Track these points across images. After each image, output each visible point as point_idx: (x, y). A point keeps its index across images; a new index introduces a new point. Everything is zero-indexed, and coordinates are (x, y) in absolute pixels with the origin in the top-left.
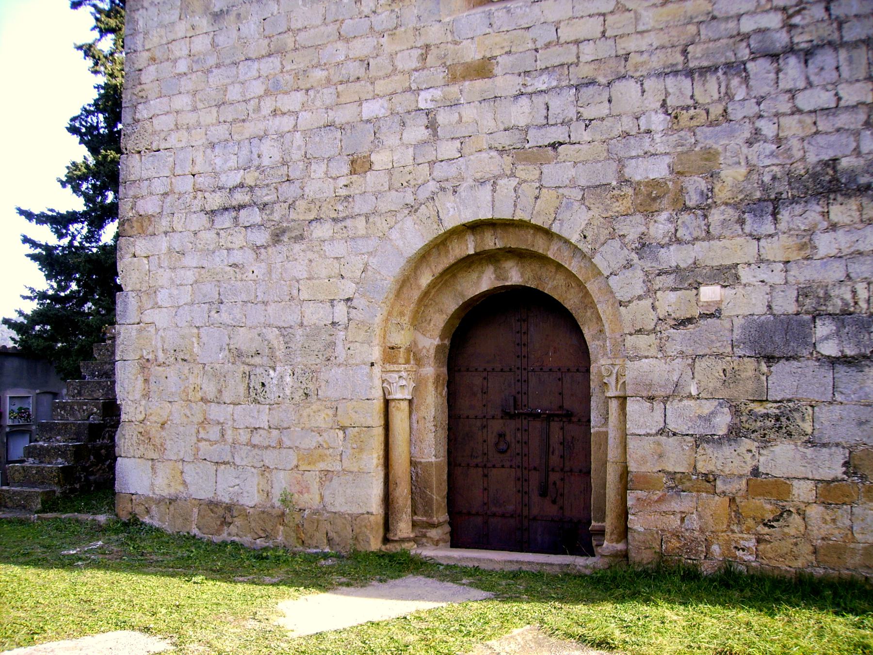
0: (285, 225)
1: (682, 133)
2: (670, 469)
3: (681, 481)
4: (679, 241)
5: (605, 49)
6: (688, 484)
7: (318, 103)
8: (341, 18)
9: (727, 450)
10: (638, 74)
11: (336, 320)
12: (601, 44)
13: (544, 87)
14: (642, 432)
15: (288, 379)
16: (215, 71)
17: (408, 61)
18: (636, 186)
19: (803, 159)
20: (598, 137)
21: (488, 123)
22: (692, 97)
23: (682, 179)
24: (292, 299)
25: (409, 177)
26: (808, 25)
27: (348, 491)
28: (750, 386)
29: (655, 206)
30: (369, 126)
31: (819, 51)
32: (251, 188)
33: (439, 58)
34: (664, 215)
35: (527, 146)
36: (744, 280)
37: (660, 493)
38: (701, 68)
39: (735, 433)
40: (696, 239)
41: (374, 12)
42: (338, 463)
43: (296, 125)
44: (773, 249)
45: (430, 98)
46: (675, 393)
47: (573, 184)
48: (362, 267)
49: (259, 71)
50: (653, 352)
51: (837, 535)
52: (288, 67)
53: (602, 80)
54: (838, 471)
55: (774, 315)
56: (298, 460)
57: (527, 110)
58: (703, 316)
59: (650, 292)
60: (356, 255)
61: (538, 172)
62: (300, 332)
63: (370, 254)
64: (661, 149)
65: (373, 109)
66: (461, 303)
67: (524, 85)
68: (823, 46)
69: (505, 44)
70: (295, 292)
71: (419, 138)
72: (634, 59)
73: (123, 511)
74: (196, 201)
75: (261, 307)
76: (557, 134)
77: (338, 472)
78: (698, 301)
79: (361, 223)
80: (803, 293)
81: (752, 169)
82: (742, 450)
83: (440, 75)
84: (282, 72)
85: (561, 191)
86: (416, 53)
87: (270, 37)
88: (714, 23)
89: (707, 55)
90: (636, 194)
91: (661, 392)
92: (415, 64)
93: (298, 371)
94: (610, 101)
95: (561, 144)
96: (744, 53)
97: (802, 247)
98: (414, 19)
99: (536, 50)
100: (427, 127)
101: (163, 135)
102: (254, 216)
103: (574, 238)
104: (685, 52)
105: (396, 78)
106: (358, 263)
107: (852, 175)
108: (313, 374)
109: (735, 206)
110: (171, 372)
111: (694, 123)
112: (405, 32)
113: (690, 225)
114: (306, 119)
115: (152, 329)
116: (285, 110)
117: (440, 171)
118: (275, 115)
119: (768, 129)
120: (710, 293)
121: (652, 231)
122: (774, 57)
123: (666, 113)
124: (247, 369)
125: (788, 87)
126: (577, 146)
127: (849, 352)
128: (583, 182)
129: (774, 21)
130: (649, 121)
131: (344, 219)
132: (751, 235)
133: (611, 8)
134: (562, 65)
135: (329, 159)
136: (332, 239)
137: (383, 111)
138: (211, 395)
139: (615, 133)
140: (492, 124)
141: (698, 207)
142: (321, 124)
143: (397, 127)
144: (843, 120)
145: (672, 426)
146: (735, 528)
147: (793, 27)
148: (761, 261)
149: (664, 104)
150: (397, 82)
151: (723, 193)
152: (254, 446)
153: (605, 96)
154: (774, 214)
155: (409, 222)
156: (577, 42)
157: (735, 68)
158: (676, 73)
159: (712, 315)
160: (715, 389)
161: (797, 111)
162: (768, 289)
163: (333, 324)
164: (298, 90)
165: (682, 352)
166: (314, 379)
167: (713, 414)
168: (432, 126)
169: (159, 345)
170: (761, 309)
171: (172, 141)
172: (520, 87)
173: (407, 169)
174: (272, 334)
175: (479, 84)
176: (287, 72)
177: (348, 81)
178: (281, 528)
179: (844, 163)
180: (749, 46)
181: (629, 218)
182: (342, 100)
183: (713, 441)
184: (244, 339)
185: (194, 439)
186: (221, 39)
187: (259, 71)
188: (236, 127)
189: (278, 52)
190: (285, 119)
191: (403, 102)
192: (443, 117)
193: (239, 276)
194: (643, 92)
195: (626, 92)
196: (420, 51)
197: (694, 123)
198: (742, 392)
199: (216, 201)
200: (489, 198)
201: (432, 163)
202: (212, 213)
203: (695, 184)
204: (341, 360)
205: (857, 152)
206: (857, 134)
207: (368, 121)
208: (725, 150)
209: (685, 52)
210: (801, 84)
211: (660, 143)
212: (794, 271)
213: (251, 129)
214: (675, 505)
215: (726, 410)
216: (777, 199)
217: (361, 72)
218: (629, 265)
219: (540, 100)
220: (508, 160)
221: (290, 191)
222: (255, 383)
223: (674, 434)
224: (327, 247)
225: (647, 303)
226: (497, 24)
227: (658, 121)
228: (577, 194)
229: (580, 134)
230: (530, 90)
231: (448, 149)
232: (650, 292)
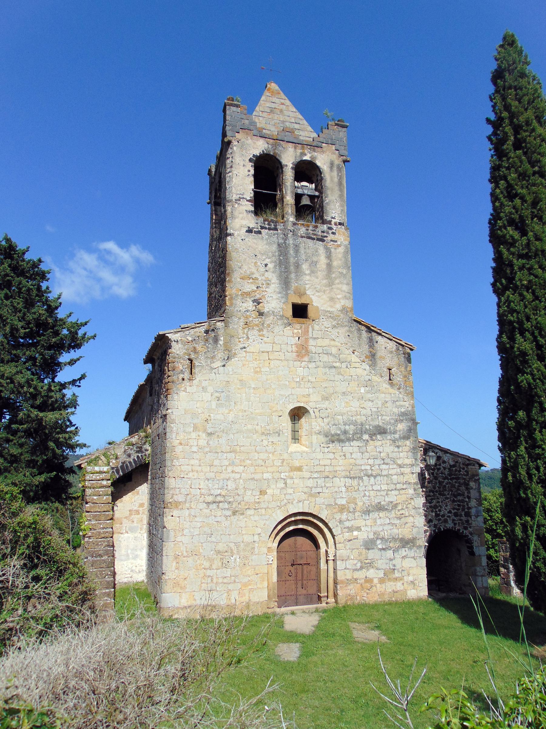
5: (331, 469)
7: (248, 471)
9: (360, 572)
15: (238, 560)
16: (209, 454)
28: (364, 556)
32: (224, 496)
33: (287, 463)
34: (345, 513)
39: (361, 568)
44: (369, 523)
47: (323, 504)
49: (226, 457)
50: (343, 548)
51: (383, 590)
52: (237, 457)
54: (383, 575)
58: (354, 539)
62: (242, 544)
63: (266, 520)
64: (344, 496)
65: (266, 476)
72: (338, 472)
73: (166, 614)
74: (201, 499)
75: (228, 536)
76: (319, 490)
79: (263, 511)
80: (375, 533)
83: (288, 469)
86: (280, 461)
89: (355, 474)
92: (280, 464)
97: (374, 522)
101: (186, 473)
102: (226, 506)
104: (349, 472)
107: (384, 506)
108: (246, 558)
110: (190, 560)
113: (351, 516)
115: (181, 544)
117: (288, 497)
119: (367, 494)
120: (355, 533)
122: (369, 476)
124: (222, 557)
127: (384, 547)
128: (326, 503)
131: (258, 509)
135: (253, 490)
136: (254, 515)
138: (207, 566)
140: (302, 485)
144: (382, 493)
151: (358, 509)
152: (225, 583)
155: (279, 511)
156: (325, 466)
157: (361, 478)
158: (348, 477)
161: (373, 490)
164: (241, 466)
168: (285, 483)
169: (185, 550)
171: (190, 475)
174: (232, 545)
175: (299, 473)
179: (382, 503)
184: (221, 547)
185: (200, 583)
186: (211, 443)
187: (226, 457)
188: (217, 474)
190: (237, 474)
191: (277, 475)
192: (288, 481)
193: (219, 525)
195: (336, 480)
198: (362, 558)
199: (210, 499)
202: (208, 503)
203: (352, 506)
204: (256, 553)
205: (384, 500)
206: (384, 496)
207: (265, 479)
209: (349, 472)
210: (374, 484)
212: (373, 528)
213: (223, 476)
217: (263, 464)
219: (315, 480)
221: (239, 499)
222: (225, 561)
224: (252, 517)
227: (344, 489)
228: (324, 507)
229: (325, 490)
231: (290, 491)
232: (342, 533)
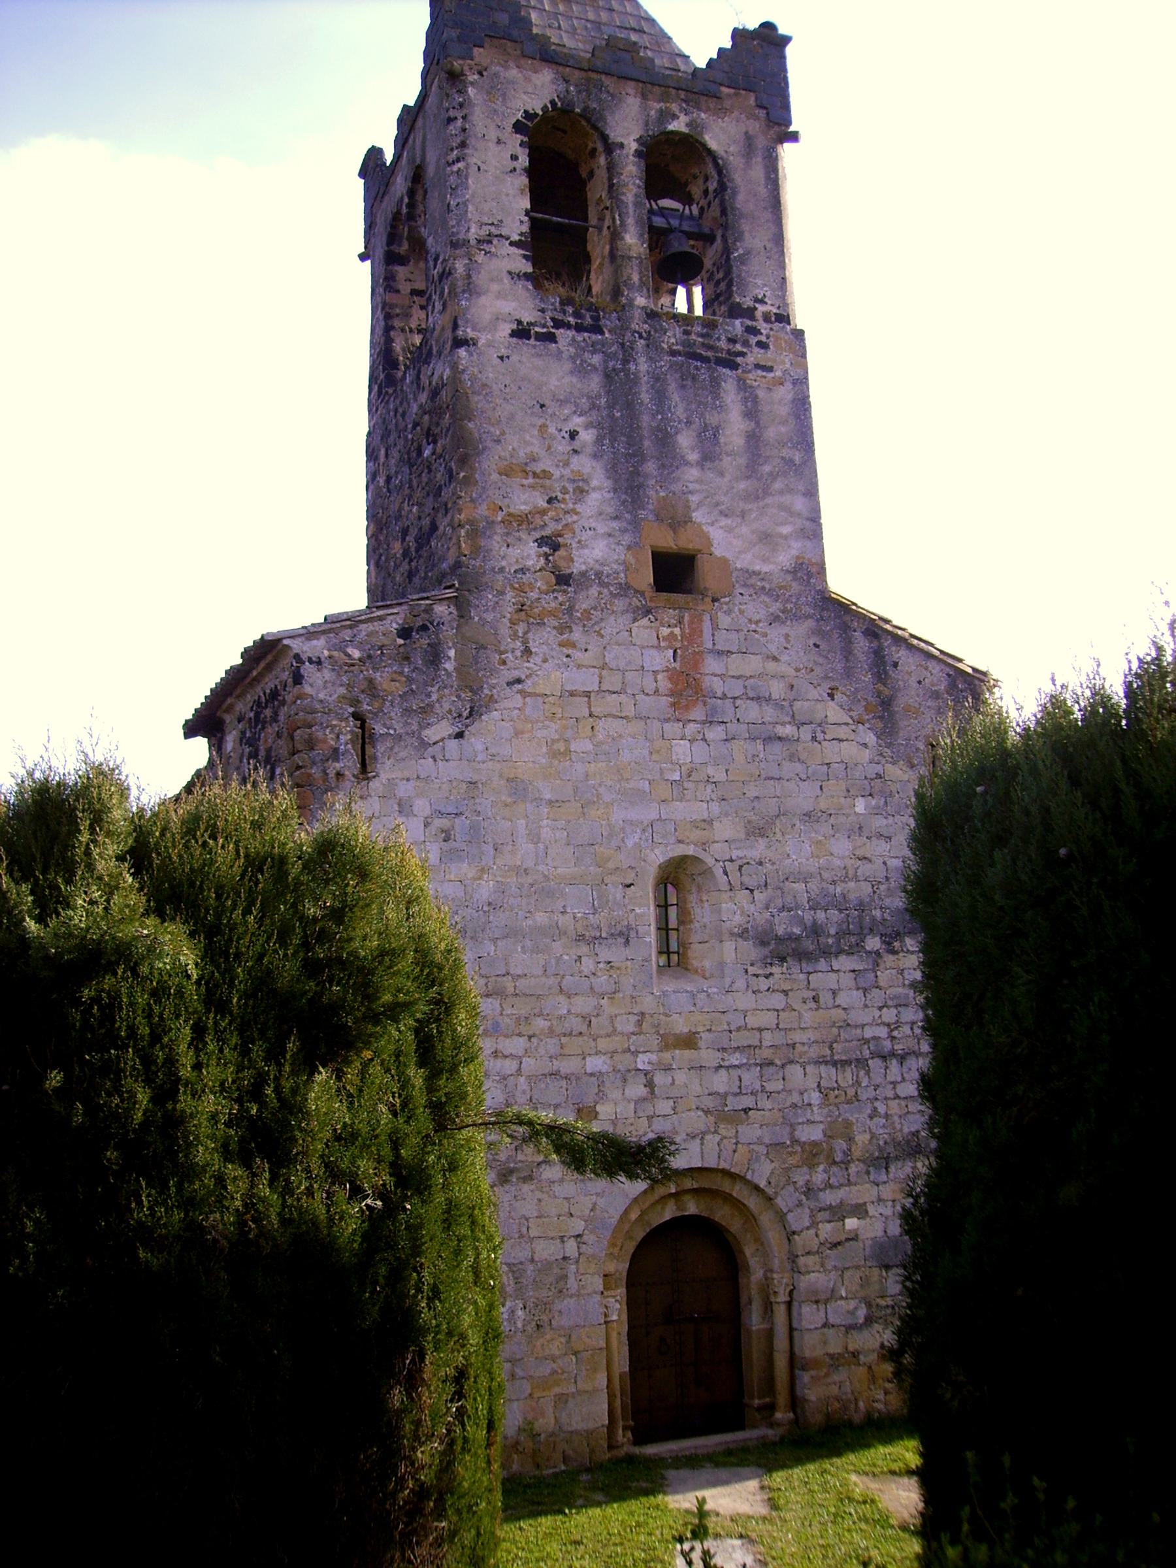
0: (512, 1165)
1: (831, 1108)
2: (831, 1351)
3: (838, 1359)
4: (831, 1187)
5: (779, 1038)
6: (843, 1361)
7: (542, 1051)
8: (561, 973)
9: (866, 1333)
10: (802, 1060)
11: (567, 1255)
12: (776, 1033)
13: (737, 1063)
14: (812, 1327)
17: (627, 1025)
18: (802, 1145)
19: (901, 1130)
20: (776, 1107)
21: (696, 1088)
22: (836, 1081)
23: (831, 1141)
24: (521, 1236)
25: (631, 1128)
26: (902, 1038)
27: (584, 1410)
28: (877, 1287)
29: (816, 1161)
30: (593, 1079)
31: (908, 1057)
34: (821, 1167)
35: (726, 1109)
36: (870, 1214)
37: (825, 1370)
38: (841, 1061)
40: (841, 1185)
41: (594, 974)
42: (573, 1385)
43: (520, 1069)
45: (647, 1061)
46: (833, 1295)
47: (760, 1142)
48: (590, 1206)
50: (817, 1268)
53: (778, 1062)
55: (888, 1237)
56: (532, 1389)
57: (725, 1079)
58: (848, 1240)
59: (814, 1224)
60: (586, 1195)
61: (734, 1131)
62: (531, 1267)
64: (818, 1118)
65: (595, 1063)
66: (648, 1231)
67: (723, 1059)
68: (910, 1054)
69: (706, 1023)
70: (524, 1230)
71: (639, 1094)
72: (799, 1048)
76: (747, 1101)
77: (573, 1393)
78: (844, 1229)
81: (873, 1136)
82: (874, 1332)
83: (655, 1042)
84: (502, 1014)
85: (751, 1146)
87: (487, 977)
88: (849, 1028)
90: (803, 1151)
91: (823, 1297)
93: (530, 1304)
94: (784, 1079)
95: (750, 1109)
96: (866, 1053)
98: (631, 988)
99: (730, 1032)
100: (645, 1086)
103: (762, 1184)
104: (831, 1048)
105: (617, 1038)
106: (587, 1202)
109: (864, 1162)
111: (837, 1101)
112: (623, 998)
114: (529, 1063)
116: (507, 1053)
118: (496, 1057)
119: (882, 1109)
120: (851, 1223)
121: (814, 1178)
122: (884, 1058)
123: (820, 1091)
125: (892, 1080)
126: (762, 1112)
128: (767, 1140)
129: (882, 1032)
130: (809, 1098)
132: (874, 1182)
133: (782, 1007)
134: (749, 1046)
136: (562, 1181)
137: (606, 1066)
139: (788, 1104)
141: (842, 1162)
142: (546, 1072)
143: (619, 1083)
145: (831, 1321)
146: (872, 1387)
147: (894, 1038)
148: (880, 1200)
149: (819, 1085)
150: (617, 1042)
151: (857, 1153)
153: (781, 1074)
154: (886, 1168)
156: (760, 1030)
157: (861, 1063)
158: (826, 1063)
159: (852, 1239)
160: (857, 1291)
161: (897, 1097)
162: (884, 1219)
163: (564, 1258)
164: (520, 1035)
165: (835, 1266)
166: (547, 1311)
167: (856, 1308)
168: (650, 1085)
170: (880, 1233)
172: (720, 1060)
173: (629, 1121)
175: (688, 1053)
176: (508, 1015)
177: (570, 1034)
178: (516, 1456)
180: (869, 1048)
181: (799, 1170)
182: (566, 1051)
183: (858, 1328)
189: (497, 994)
190: (507, 1062)
191: (624, 1061)
192: (659, 1079)
194: (805, 1074)
195: (795, 1071)
196: (636, 1018)
197: (837, 1101)
200: (699, 1150)
201: (650, 1118)
203: (840, 1144)
204: (573, 1291)
207: (592, 1075)
208: (857, 1121)
209: (831, 1048)
210: (899, 1079)
211: (817, 1114)
214: (836, 1378)
215: (863, 1305)
216: (888, 1157)
217: (584, 1028)
218: (800, 1204)
219: (735, 1073)
220: (712, 1119)
223: (833, 1326)
224: (556, 1188)
225: (812, 1232)
226: (700, 1003)
227: (815, 1098)
228: (762, 1149)
230: (727, 1063)
231: (664, 1107)
232: (814, 1224)
